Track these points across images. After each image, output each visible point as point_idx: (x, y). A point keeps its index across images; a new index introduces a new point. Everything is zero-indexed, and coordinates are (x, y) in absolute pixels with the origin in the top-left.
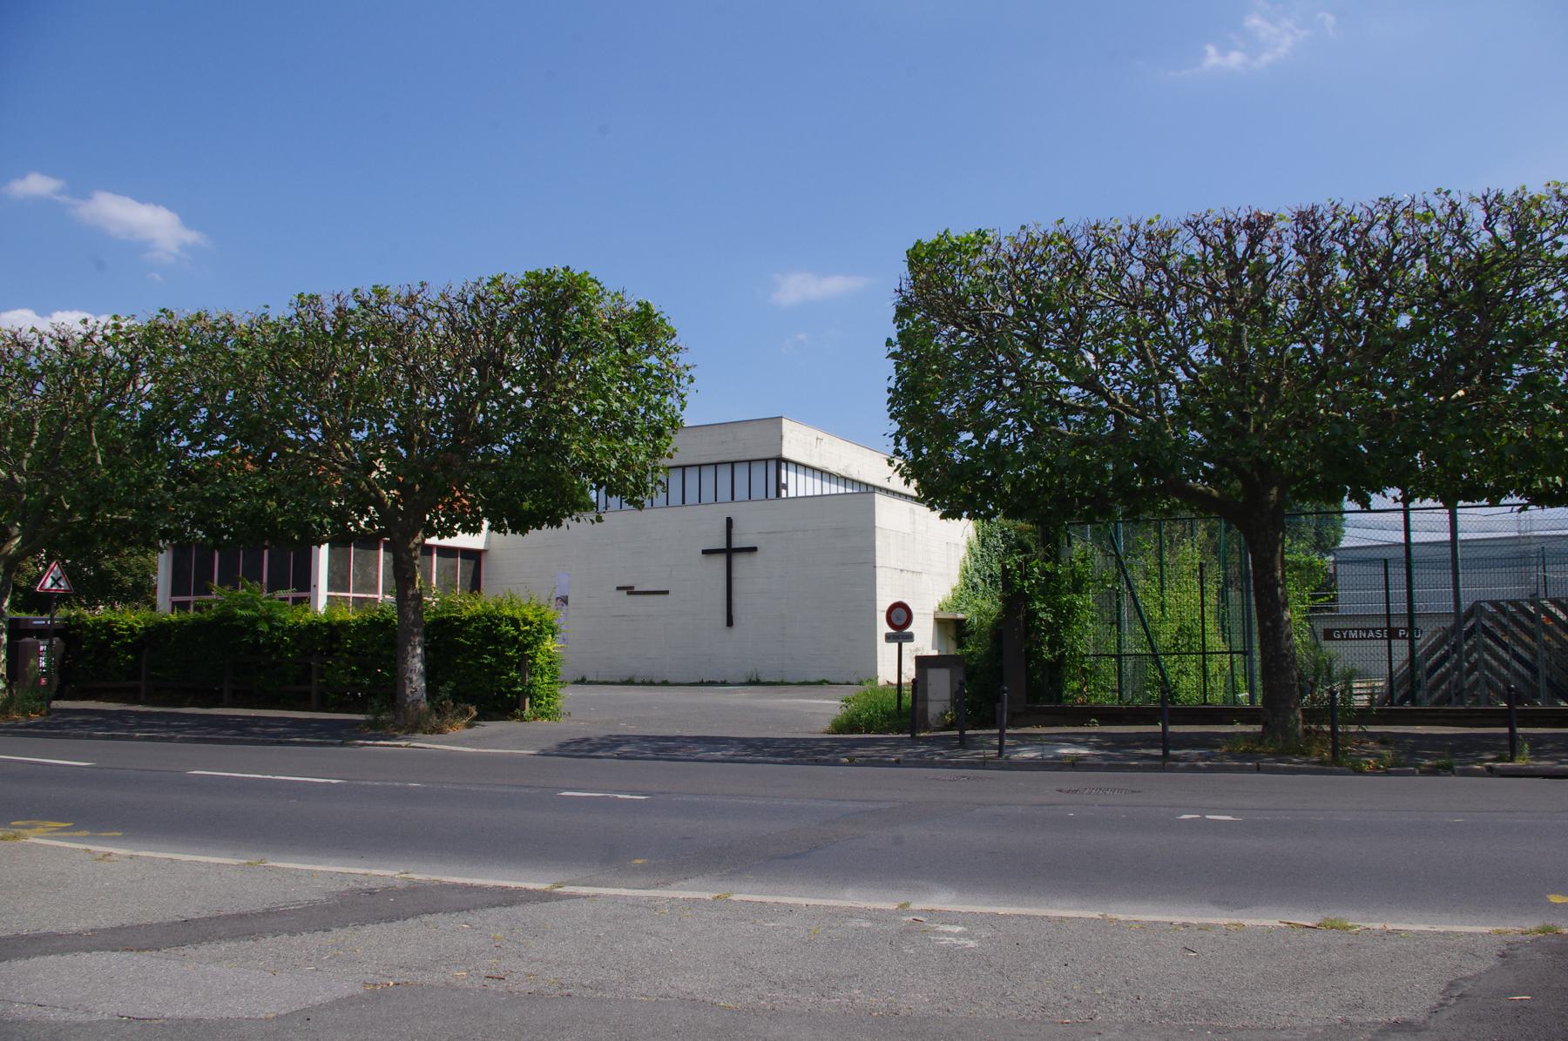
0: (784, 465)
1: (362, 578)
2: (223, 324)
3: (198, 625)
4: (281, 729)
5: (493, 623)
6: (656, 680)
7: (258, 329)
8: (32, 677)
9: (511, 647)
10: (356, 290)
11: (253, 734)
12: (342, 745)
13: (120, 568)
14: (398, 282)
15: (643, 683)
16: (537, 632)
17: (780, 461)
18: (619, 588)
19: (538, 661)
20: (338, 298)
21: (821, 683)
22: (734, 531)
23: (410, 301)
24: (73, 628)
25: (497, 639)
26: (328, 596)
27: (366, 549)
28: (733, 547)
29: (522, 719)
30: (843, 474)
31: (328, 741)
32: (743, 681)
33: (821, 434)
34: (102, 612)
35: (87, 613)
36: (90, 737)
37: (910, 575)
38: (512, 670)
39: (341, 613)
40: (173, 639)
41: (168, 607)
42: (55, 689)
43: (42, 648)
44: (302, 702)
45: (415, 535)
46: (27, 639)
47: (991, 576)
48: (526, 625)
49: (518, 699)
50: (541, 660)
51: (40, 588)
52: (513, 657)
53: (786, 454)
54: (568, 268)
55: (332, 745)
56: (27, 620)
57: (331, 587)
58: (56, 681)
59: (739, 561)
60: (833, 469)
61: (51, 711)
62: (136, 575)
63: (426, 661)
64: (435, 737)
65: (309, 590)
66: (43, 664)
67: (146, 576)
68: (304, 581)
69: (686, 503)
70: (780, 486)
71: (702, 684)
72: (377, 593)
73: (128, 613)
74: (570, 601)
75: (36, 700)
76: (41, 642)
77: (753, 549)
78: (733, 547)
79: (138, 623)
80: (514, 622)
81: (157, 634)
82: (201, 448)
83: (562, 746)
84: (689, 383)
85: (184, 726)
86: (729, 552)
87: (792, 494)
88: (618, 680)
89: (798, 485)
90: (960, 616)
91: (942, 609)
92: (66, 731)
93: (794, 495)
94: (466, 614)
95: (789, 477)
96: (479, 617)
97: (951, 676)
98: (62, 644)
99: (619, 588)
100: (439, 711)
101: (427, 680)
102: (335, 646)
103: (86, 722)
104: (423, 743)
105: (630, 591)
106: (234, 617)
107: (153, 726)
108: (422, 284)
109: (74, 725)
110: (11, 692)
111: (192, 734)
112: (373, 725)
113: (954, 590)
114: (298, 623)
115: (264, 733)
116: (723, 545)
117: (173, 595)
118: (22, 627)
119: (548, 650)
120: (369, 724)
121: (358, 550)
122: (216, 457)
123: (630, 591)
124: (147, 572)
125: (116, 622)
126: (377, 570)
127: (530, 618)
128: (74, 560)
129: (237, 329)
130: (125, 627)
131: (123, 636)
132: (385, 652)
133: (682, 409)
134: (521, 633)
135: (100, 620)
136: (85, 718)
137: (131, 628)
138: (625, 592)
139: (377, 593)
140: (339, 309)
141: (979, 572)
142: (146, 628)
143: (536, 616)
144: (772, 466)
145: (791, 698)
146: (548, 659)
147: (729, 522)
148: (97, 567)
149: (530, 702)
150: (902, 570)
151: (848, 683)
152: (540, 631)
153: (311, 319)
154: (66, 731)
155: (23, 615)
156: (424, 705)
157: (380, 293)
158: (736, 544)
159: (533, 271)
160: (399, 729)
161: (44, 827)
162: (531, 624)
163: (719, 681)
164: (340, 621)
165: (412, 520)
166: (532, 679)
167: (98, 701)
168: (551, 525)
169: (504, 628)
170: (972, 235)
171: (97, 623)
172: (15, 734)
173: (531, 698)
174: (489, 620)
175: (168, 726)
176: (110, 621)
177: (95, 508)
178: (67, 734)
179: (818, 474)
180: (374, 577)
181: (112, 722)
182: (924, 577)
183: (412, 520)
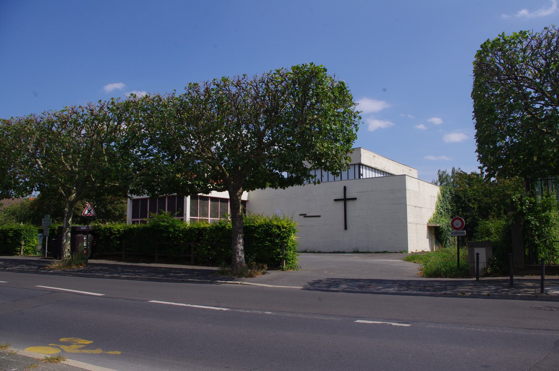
0: (361, 166)
1: (202, 212)
2: (156, 99)
3: (145, 229)
4: (182, 274)
5: (269, 228)
6: (316, 251)
7: (171, 100)
8: (80, 251)
9: (277, 238)
10: (214, 80)
11: (170, 277)
12: (211, 283)
13: (114, 208)
14: (233, 75)
15: (311, 252)
16: (288, 232)
17: (360, 165)
18: (300, 215)
19: (289, 244)
20: (206, 84)
21: (385, 252)
22: (347, 192)
23: (238, 84)
24: (96, 230)
25: (271, 235)
26: (190, 218)
28: (347, 198)
29: (283, 270)
30: (383, 170)
31: (205, 281)
32: (352, 251)
33: (375, 155)
34: (108, 225)
35: (102, 225)
36: (103, 277)
37: (418, 209)
38: (278, 248)
39: (203, 224)
40: (135, 235)
41: (131, 222)
42: (89, 256)
43: (85, 238)
44: (187, 261)
45: (239, 189)
46: (79, 235)
47: (447, 209)
48: (283, 228)
49: (281, 261)
50: (290, 244)
51: (83, 214)
52: (278, 243)
53: (363, 162)
54: (312, 63)
55: (206, 283)
56: (79, 227)
57: (191, 215)
58: (90, 252)
59: (349, 204)
60: (379, 168)
61: (88, 264)
62: (120, 211)
63: (245, 245)
64: (251, 279)
65: (183, 216)
66: (85, 245)
67: (123, 211)
68: (182, 214)
69: (323, 181)
70: (360, 175)
71: (334, 252)
72: (208, 217)
73: (117, 225)
75: (81, 260)
76: (84, 236)
77: (355, 199)
78: (347, 198)
79: (121, 228)
80: (278, 227)
81: (129, 232)
82: (146, 156)
83: (312, 284)
84: (359, 120)
85: (142, 272)
86: (345, 200)
87: (364, 177)
88: (300, 251)
89: (366, 174)
90: (438, 225)
91: (430, 222)
92: (93, 274)
93: (371, 177)
94: (257, 224)
95: (364, 171)
96: (263, 225)
97: (486, 251)
98: (92, 237)
99: (300, 215)
100: (250, 267)
101: (246, 254)
102: (201, 238)
103: (102, 270)
104: (246, 282)
105: (305, 216)
106: (159, 226)
107: (129, 272)
108: (244, 75)
109: (97, 271)
110: (72, 257)
111: (145, 276)
112: (222, 273)
113: (434, 215)
114: (185, 228)
115: (175, 276)
117: (132, 218)
118: (77, 230)
119: (292, 240)
120: (222, 273)
121: (201, 201)
122: (152, 159)
123: (305, 216)
124: (124, 211)
125: (113, 228)
126: (208, 209)
127: (285, 226)
128: (98, 206)
129: (163, 101)
130: (116, 230)
131: (115, 234)
132: (222, 240)
133: (357, 131)
134: (282, 232)
135: (107, 227)
136: (101, 267)
137: (119, 231)
138: (303, 216)
139: (208, 217)
140: (207, 89)
141: (442, 208)
142: (124, 231)
143: (287, 225)
145: (379, 259)
146: (292, 243)
147: (345, 188)
148: (105, 209)
149: (286, 262)
150: (416, 207)
151: (396, 252)
152: (289, 231)
153: (194, 94)
154: (93, 274)
155: (78, 225)
156: (244, 264)
157: (225, 80)
158: (348, 196)
159: (296, 65)
160: (235, 275)
161: (77, 344)
162: (286, 228)
163: (342, 251)
164: (203, 228)
165: (238, 182)
166: (286, 252)
167: (106, 260)
168: (292, 186)
169: (274, 230)
170: (518, 34)
171: (106, 228)
172: (73, 275)
173: (286, 260)
174: (267, 226)
175: (135, 272)
176: (110, 228)
177: (104, 180)
178: (93, 275)
179: (373, 170)
180: (207, 211)
181: (111, 270)
182: (423, 209)
183: (238, 182)
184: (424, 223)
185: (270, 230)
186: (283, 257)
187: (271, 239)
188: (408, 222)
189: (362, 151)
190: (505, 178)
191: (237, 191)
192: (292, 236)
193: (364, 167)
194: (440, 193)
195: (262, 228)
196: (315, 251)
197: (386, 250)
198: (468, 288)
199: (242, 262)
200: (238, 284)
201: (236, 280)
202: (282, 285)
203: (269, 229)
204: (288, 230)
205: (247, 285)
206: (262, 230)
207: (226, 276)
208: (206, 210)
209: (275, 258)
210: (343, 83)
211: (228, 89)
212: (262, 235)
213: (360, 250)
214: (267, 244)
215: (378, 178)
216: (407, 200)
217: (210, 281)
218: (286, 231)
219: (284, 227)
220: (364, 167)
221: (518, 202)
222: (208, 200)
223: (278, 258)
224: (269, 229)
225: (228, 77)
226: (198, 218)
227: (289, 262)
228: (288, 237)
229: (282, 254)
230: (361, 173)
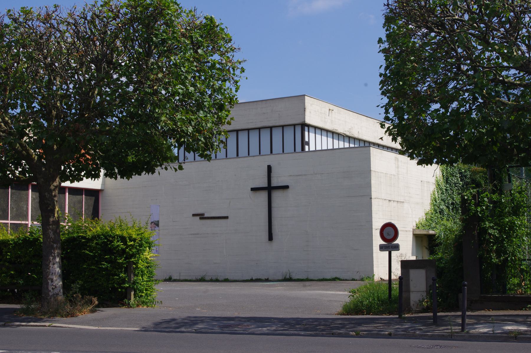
0: (306, 128)
5: (108, 240)
9: (121, 256)
15: (211, 281)
17: (304, 126)
18: (194, 215)
19: (139, 266)
21: (334, 279)
22: (273, 174)
27: (19, 190)
29: (129, 306)
30: (348, 134)
32: (280, 278)
33: (332, 107)
37: (395, 204)
38: (121, 272)
45: (54, 180)
47: (452, 204)
48: (131, 241)
50: (141, 265)
53: (308, 121)
59: (277, 195)
60: (340, 130)
63: (63, 267)
64: (69, 319)
70: (304, 143)
71: (252, 280)
74: (160, 224)
77: (286, 187)
80: (123, 239)
86: (270, 189)
87: (312, 148)
88: (194, 278)
90: (431, 232)
91: (418, 228)
95: (311, 137)
96: (99, 236)
99: (194, 215)
100: (72, 301)
105: (202, 217)
108: (56, 6)
112: (25, 312)
113: (426, 214)
116: (265, 185)
119: (147, 258)
120: (25, 312)
121: (14, 191)
123: (202, 217)
126: (27, 205)
127: (134, 236)
132: (34, 261)
133: (236, 91)
138: (198, 218)
139: (28, 221)
141: (444, 202)
143: (138, 235)
144: (298, 130)
145: (314, 290)
146: (146, 265)
147: (269, 168)
149: (134, 294)
150: (385, 199)
152: (141, 245)
156: (61, 298)
157: (26, 12)
158: (274, 183)
160: (45, 314)
162: (134, 240)
165: (52, 170)
166: (135, 278)
169: (116, 243)
173: (135, 291)
174: (106, 238)
179: (330, 135)
180: (25, 209)
182: (406, 205)
183: (52, 170)
184: (407, 229)
185: (109, 244)
186: (129, 286)
187: (111, 257)
188: (373, 227)
189: (308, 101)
190: (472, 164)
191: (51, 183)
192: (146, 253)
193: (311, 129)
194: (441, 175)
195: (97, 240)
196: (219, 278)
197: (338, 276)
198: (371, 327)
199: (57, 294)
200: (45, 326)
201: (45, 321)
202: (112, 327)
203: (108, 241)
204: (138, 243)
205: (58, 327)
206: (97, 244)
207: (31, 317)
208: (23, 207)
209: (118, 288)
210: (211, 20)
211: (31, 25)
212: (97, 252)
213: (295, 277)
214: (104, 266)
215: (328, 151)
216: (373, 189)
217: (3, 323)
218: (134, 245)
219: (131, 239)
220: (311, 129)
221: (471, 200)
222: (28, 190)
223: (122, 288)
224: (108, 241)
225: (31, 8)
226: (9, 222)
227: (140, 294)
228: (139, 254)
229: (129, 282)
230: (307, 139)
